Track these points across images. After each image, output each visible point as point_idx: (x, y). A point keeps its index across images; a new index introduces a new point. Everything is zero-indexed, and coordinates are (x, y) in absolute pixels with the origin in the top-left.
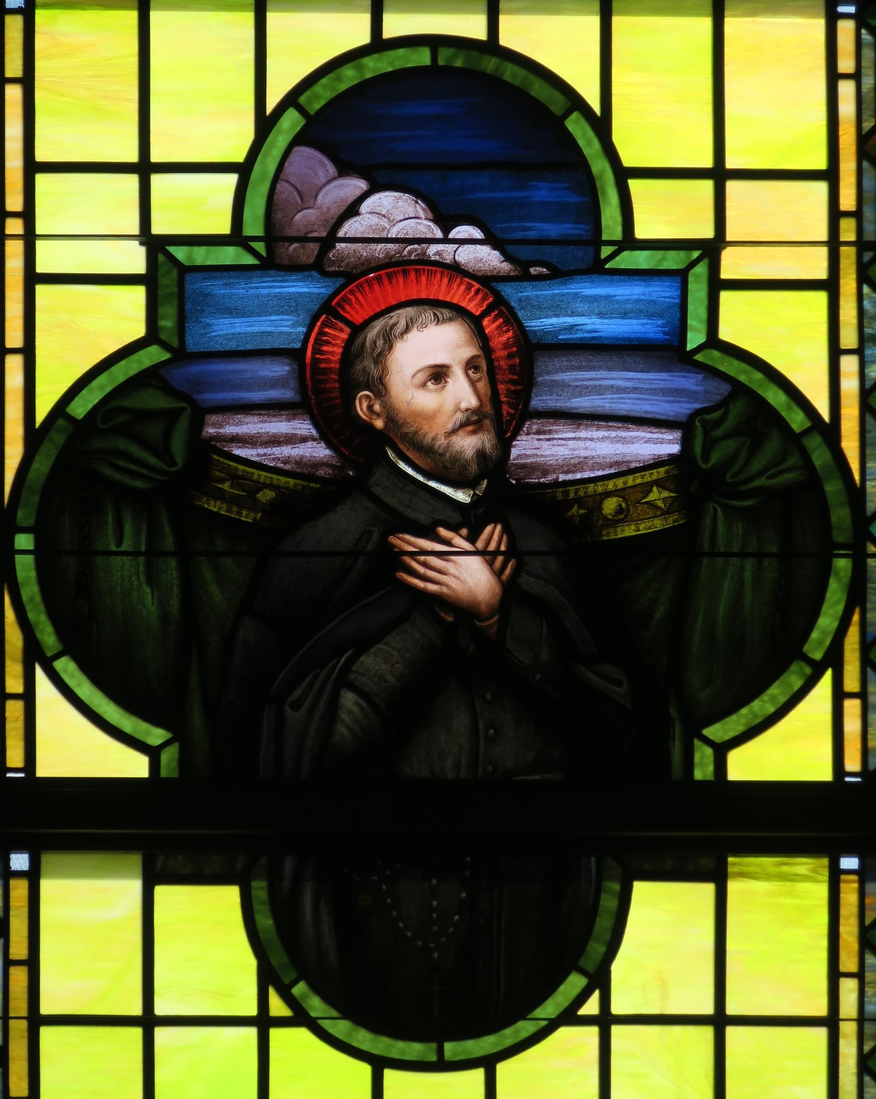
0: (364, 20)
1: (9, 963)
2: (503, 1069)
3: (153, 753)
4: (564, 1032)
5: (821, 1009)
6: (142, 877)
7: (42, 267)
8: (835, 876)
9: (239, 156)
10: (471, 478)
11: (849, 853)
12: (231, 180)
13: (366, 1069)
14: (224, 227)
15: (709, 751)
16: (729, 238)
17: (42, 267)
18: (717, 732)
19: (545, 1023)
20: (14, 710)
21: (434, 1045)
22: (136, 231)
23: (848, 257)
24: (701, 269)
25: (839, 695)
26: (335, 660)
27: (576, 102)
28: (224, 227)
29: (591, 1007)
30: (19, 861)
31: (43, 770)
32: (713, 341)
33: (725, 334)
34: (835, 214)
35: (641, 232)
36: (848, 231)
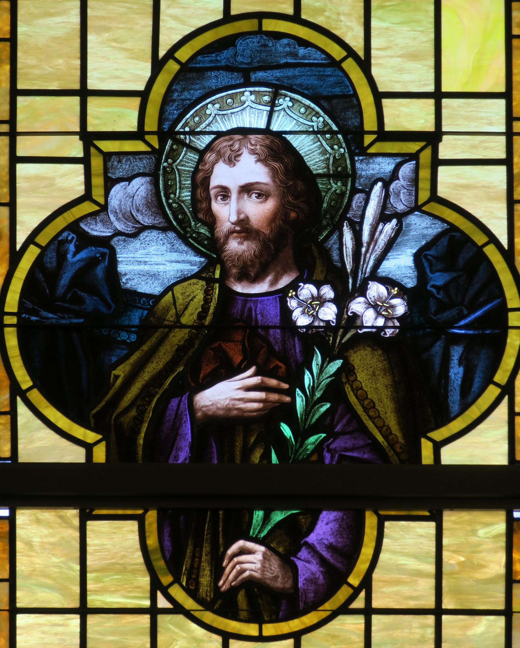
2: (304, 639)
3: (89, 448)
6: (513, 559)
7: (20, 153)
9: (141, 87)
10: (416, 213)
12: (136, 101)
13: (218, 640)
15: (430, 444)
17: (20, 153)
18: (439, 435)
22: (78, 129)
29: (359, 603)
31: (24, 457)
33: (442, 192)
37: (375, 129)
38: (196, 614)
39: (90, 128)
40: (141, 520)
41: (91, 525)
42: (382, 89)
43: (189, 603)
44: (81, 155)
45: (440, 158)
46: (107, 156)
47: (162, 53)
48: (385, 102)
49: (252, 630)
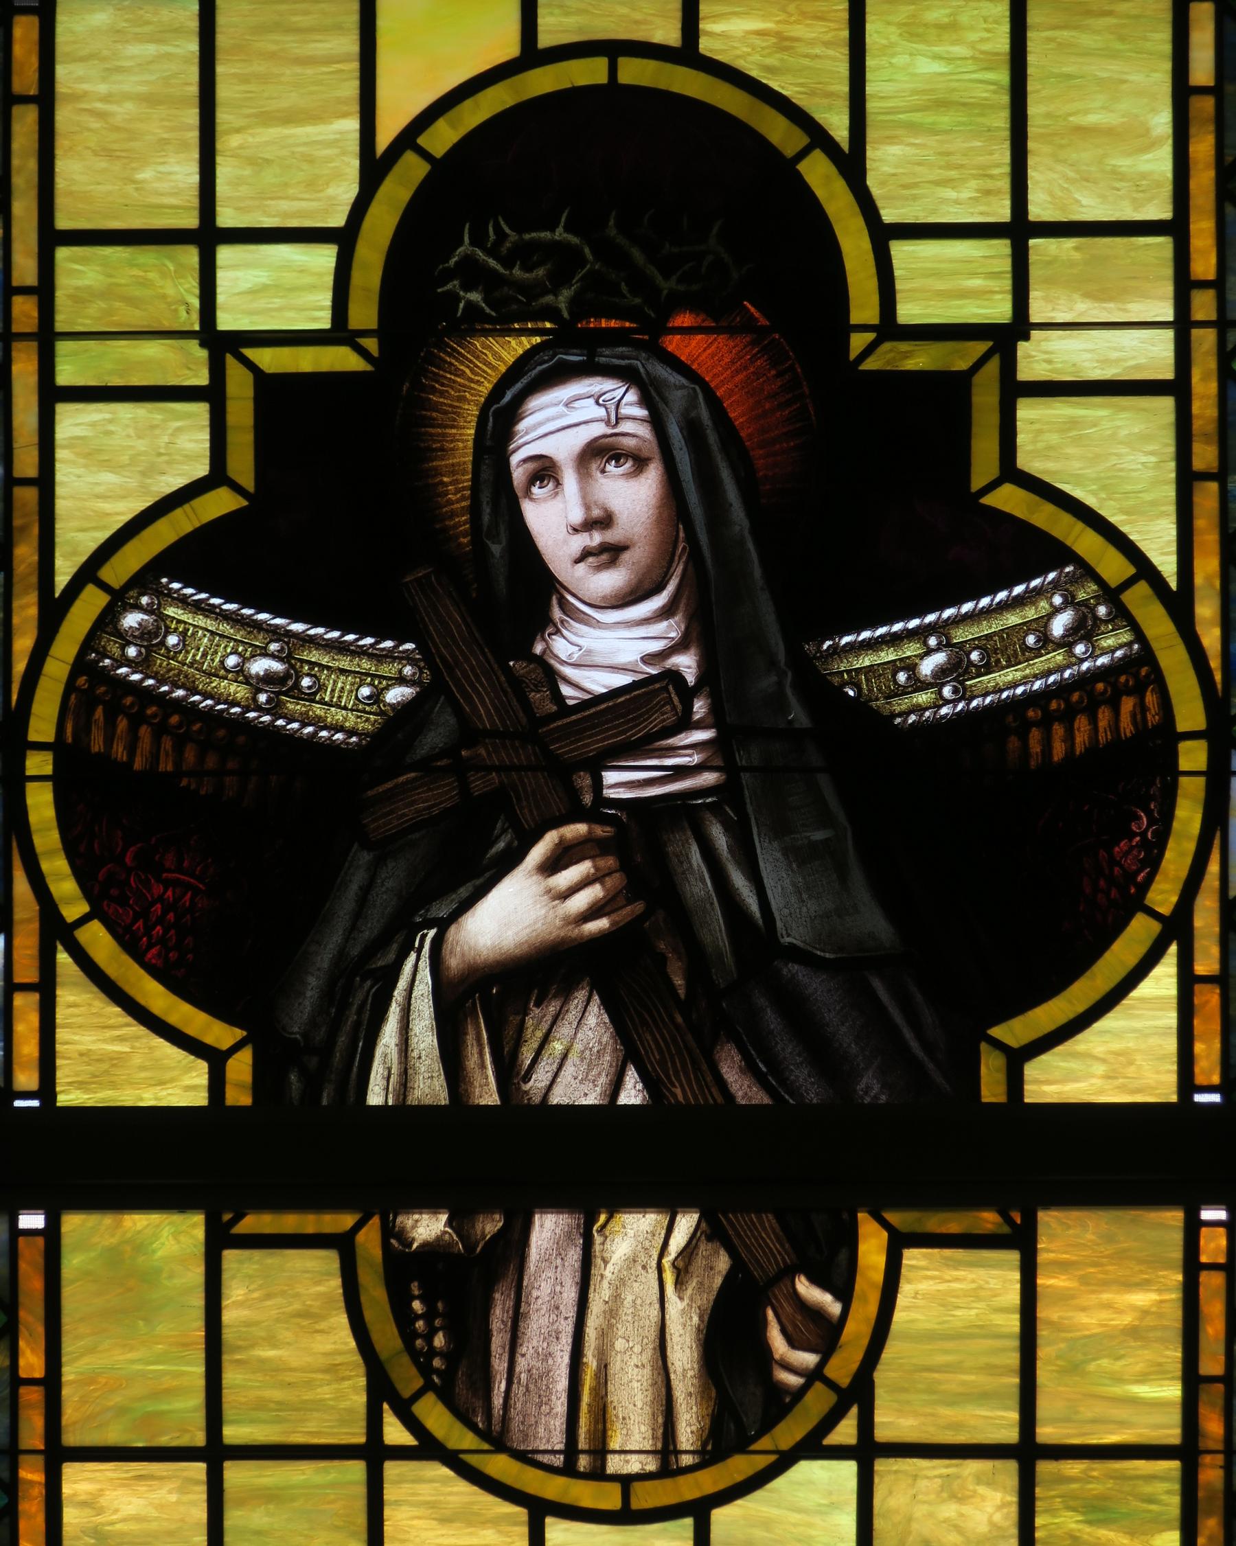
0: (689, 1448)
1: (12, 988)
3: (216, 1060)
4: (807, 1470)
5: (1172, 1434)
8: (1193, 1228)
9: (338, 220)
11: (1213, 1202)
12: (324, 257)
14: (323, 321)
15: (225, 1045)
16: (1035, 317)
18: (1014, 1032)
19: (773, 1458)
20: (26, 1007)
21: (1222, 1259)
23: (1205, 342)
24: (993, 367)
25: (1187, 980)
26: (21, 886)
27: (819, 137)
28: (323, 321)
29: (846, 1432)
30: (32, 1221)
32: (1010, 472)
33: (1027, 461)
34: (1184, 285)
35: (909, 312)
36: (1204, 306)
37: (875, 320)
38: (472, 1460)
39: (226, 321)
40: (344, 1245)
41: (231, 1258)
42: (889, 215)
43: (461, 1438)
44: (201, 378)
45: (1007, 242)
46: (265, 383)
47: (383, 140)
48: (901, 251)
49: (633, 72)
